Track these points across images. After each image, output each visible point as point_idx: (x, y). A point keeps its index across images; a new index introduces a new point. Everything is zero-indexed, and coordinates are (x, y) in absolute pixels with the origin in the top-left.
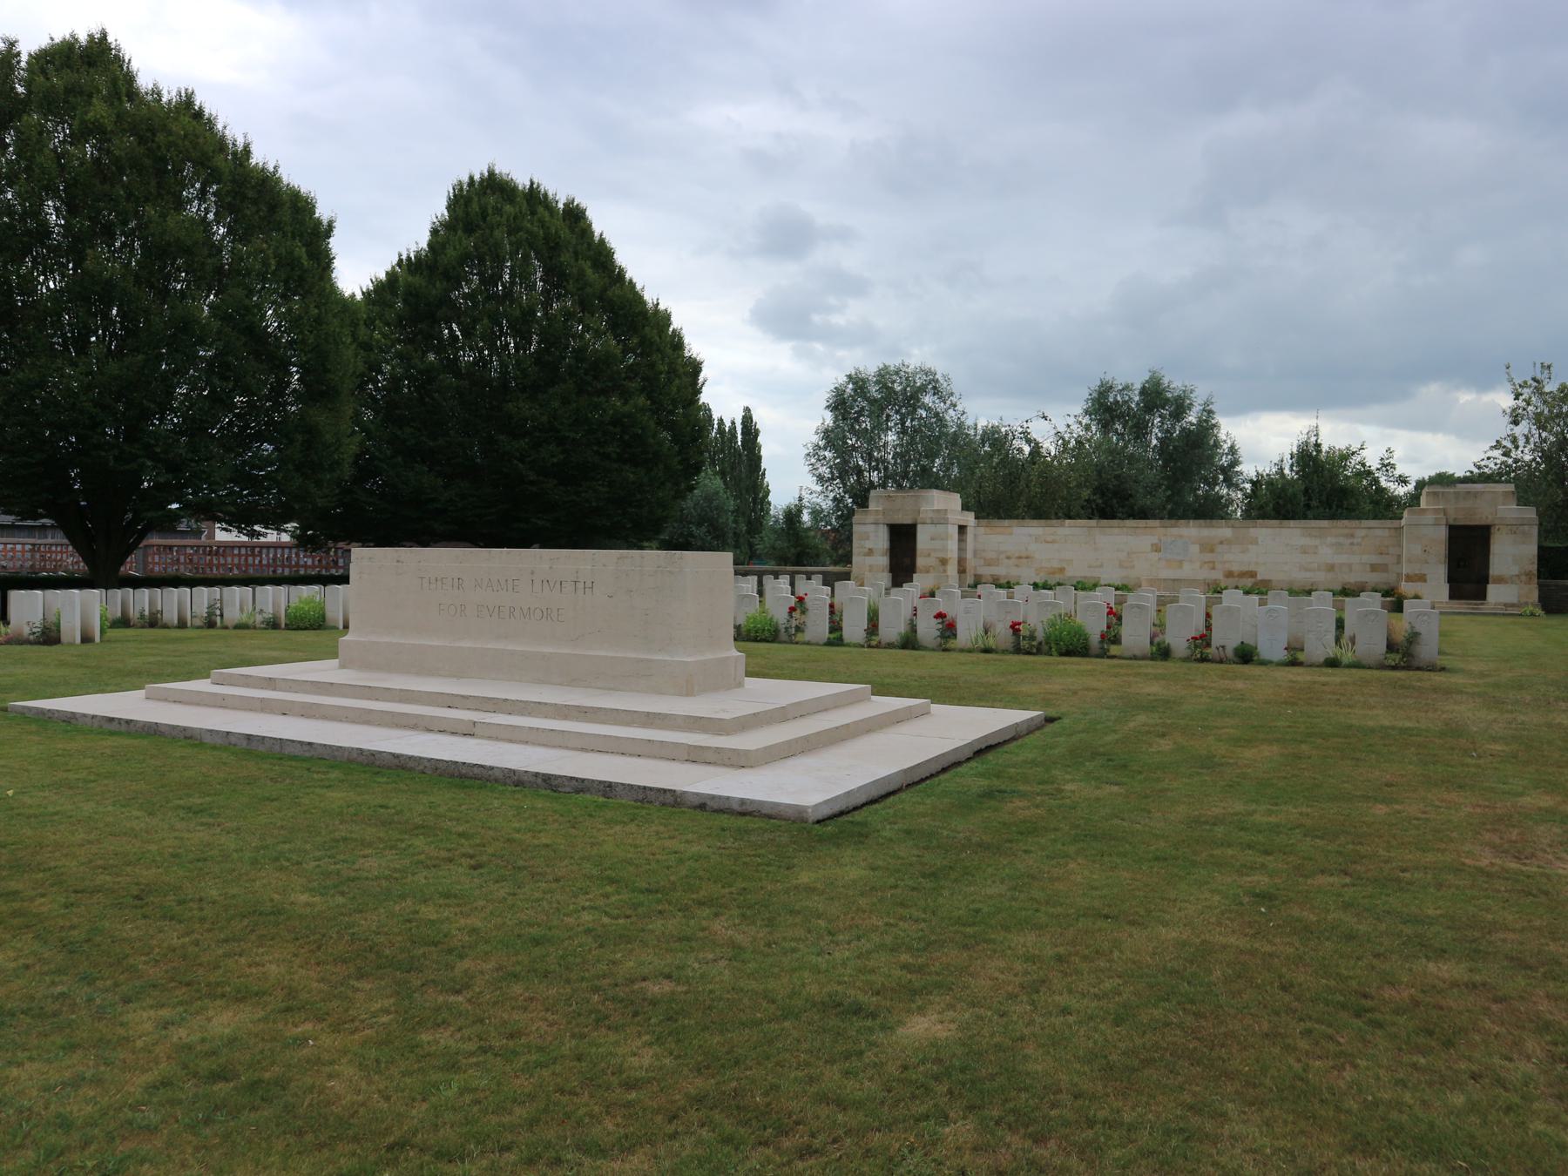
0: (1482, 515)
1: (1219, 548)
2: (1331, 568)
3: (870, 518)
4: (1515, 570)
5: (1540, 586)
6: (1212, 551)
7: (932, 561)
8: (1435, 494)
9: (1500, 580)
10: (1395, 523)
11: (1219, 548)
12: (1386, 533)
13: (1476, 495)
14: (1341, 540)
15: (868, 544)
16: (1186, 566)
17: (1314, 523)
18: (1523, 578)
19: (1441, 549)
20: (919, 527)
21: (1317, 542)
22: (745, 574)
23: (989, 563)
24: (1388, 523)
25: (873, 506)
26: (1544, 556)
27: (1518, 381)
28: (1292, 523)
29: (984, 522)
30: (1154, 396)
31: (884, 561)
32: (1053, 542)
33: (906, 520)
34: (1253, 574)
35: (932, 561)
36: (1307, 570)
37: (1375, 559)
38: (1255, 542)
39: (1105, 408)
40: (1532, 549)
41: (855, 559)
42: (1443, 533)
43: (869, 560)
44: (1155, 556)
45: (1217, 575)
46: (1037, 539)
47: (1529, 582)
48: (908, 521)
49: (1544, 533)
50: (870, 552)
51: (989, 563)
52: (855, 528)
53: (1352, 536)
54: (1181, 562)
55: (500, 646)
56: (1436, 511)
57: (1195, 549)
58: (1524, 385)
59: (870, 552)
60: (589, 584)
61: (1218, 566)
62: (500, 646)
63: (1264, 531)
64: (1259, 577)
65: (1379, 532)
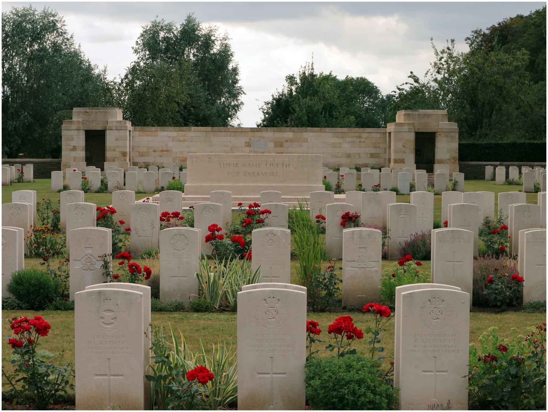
0: (431, 127)
1: (286, 145)
2: (349, 156)
3: (74, 127)
4: (447, 156)
5: (460, 165)
6: (281, 146)
7: (117, 154)
8: (408, 115)
9: (441, 162)
10: (383, 130)
11: (286, 145)
12: (378, 135)
13: (429, 116)
14: (354, 139)
15: (73, 143)
17: (339, 130)
18: (452, 161)
19: (412, 146)
20: (108, 133)
21: (341, 140)
22: (12, 164)
23: (142, 155)
24: (379, 130)
25: (75, 119)
26: (462, 148)
27: (439, 50)
28: (327, 129)
29: (138, 128)
30: (189, 34)
31: (82, 154)
32: (184, 141)
33: (99, 127)
35: (117, 154)
36: (336, 157)
37: (373, 151)
38: (306, 141)
39: (152, 42)
40: (455, 145)
41: (64, 153)
42: (412, 136)
43: (73, 154)
44: (248, 149)
46: (174, 139)
47: (454, 163)
48: (99, 128)
49: (461, 134)
50: (74, 149)
51: (142, 155)
52: (64, 133)
53: (360, 137)
55: (255, 184)
56: (409, 124)
57: (271, 145)
58: (443, 52)
59: (74, 149)
60: (288, 165)
62: (255, 184)
63: (311, 134)
65: (374, 135)
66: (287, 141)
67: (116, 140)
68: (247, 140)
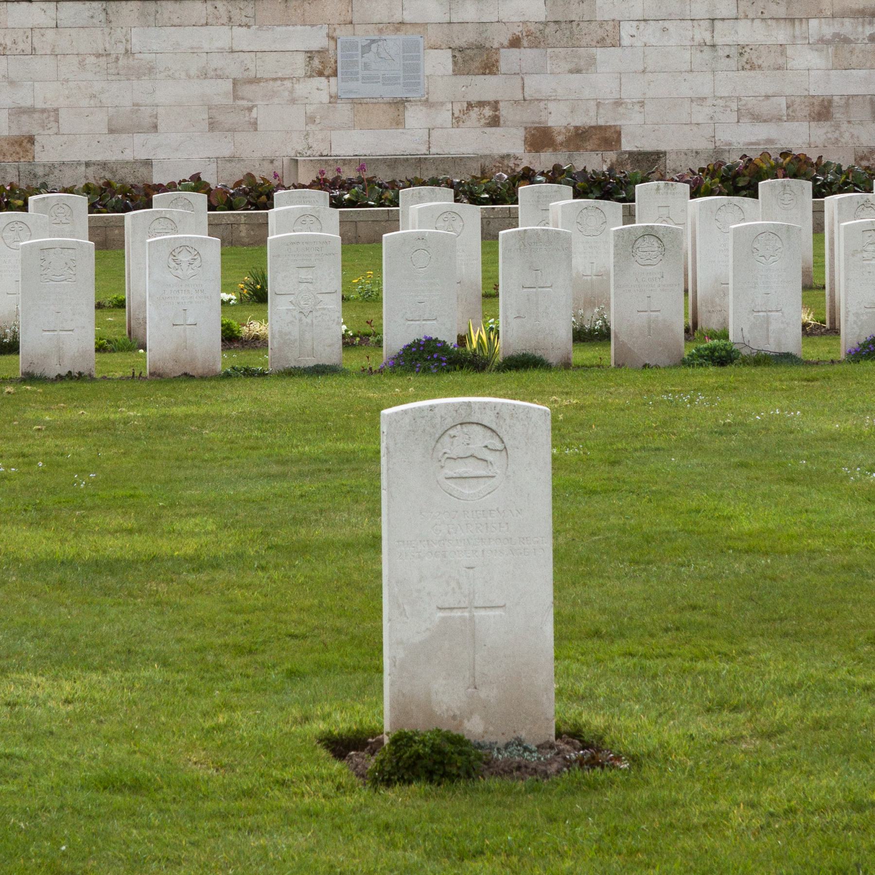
2: (823, 111)
6: (490, 68)
11: (509, 59)
16: (415, 117)
21: (781, 34)
34: (608, 138)
36: (757, 118)
44: (318, 90)
45: (508, 144)
54: (400, 104)
57: (438, 63)
61: (505, 111)
64: (627, 145)
66: (515, 43)
67: (111, 131)
68: (317, 40)
